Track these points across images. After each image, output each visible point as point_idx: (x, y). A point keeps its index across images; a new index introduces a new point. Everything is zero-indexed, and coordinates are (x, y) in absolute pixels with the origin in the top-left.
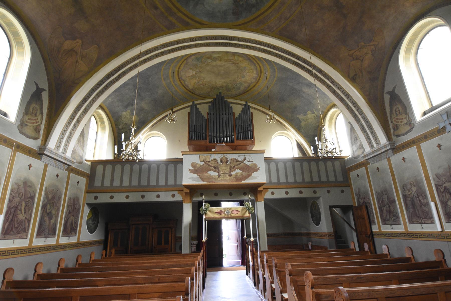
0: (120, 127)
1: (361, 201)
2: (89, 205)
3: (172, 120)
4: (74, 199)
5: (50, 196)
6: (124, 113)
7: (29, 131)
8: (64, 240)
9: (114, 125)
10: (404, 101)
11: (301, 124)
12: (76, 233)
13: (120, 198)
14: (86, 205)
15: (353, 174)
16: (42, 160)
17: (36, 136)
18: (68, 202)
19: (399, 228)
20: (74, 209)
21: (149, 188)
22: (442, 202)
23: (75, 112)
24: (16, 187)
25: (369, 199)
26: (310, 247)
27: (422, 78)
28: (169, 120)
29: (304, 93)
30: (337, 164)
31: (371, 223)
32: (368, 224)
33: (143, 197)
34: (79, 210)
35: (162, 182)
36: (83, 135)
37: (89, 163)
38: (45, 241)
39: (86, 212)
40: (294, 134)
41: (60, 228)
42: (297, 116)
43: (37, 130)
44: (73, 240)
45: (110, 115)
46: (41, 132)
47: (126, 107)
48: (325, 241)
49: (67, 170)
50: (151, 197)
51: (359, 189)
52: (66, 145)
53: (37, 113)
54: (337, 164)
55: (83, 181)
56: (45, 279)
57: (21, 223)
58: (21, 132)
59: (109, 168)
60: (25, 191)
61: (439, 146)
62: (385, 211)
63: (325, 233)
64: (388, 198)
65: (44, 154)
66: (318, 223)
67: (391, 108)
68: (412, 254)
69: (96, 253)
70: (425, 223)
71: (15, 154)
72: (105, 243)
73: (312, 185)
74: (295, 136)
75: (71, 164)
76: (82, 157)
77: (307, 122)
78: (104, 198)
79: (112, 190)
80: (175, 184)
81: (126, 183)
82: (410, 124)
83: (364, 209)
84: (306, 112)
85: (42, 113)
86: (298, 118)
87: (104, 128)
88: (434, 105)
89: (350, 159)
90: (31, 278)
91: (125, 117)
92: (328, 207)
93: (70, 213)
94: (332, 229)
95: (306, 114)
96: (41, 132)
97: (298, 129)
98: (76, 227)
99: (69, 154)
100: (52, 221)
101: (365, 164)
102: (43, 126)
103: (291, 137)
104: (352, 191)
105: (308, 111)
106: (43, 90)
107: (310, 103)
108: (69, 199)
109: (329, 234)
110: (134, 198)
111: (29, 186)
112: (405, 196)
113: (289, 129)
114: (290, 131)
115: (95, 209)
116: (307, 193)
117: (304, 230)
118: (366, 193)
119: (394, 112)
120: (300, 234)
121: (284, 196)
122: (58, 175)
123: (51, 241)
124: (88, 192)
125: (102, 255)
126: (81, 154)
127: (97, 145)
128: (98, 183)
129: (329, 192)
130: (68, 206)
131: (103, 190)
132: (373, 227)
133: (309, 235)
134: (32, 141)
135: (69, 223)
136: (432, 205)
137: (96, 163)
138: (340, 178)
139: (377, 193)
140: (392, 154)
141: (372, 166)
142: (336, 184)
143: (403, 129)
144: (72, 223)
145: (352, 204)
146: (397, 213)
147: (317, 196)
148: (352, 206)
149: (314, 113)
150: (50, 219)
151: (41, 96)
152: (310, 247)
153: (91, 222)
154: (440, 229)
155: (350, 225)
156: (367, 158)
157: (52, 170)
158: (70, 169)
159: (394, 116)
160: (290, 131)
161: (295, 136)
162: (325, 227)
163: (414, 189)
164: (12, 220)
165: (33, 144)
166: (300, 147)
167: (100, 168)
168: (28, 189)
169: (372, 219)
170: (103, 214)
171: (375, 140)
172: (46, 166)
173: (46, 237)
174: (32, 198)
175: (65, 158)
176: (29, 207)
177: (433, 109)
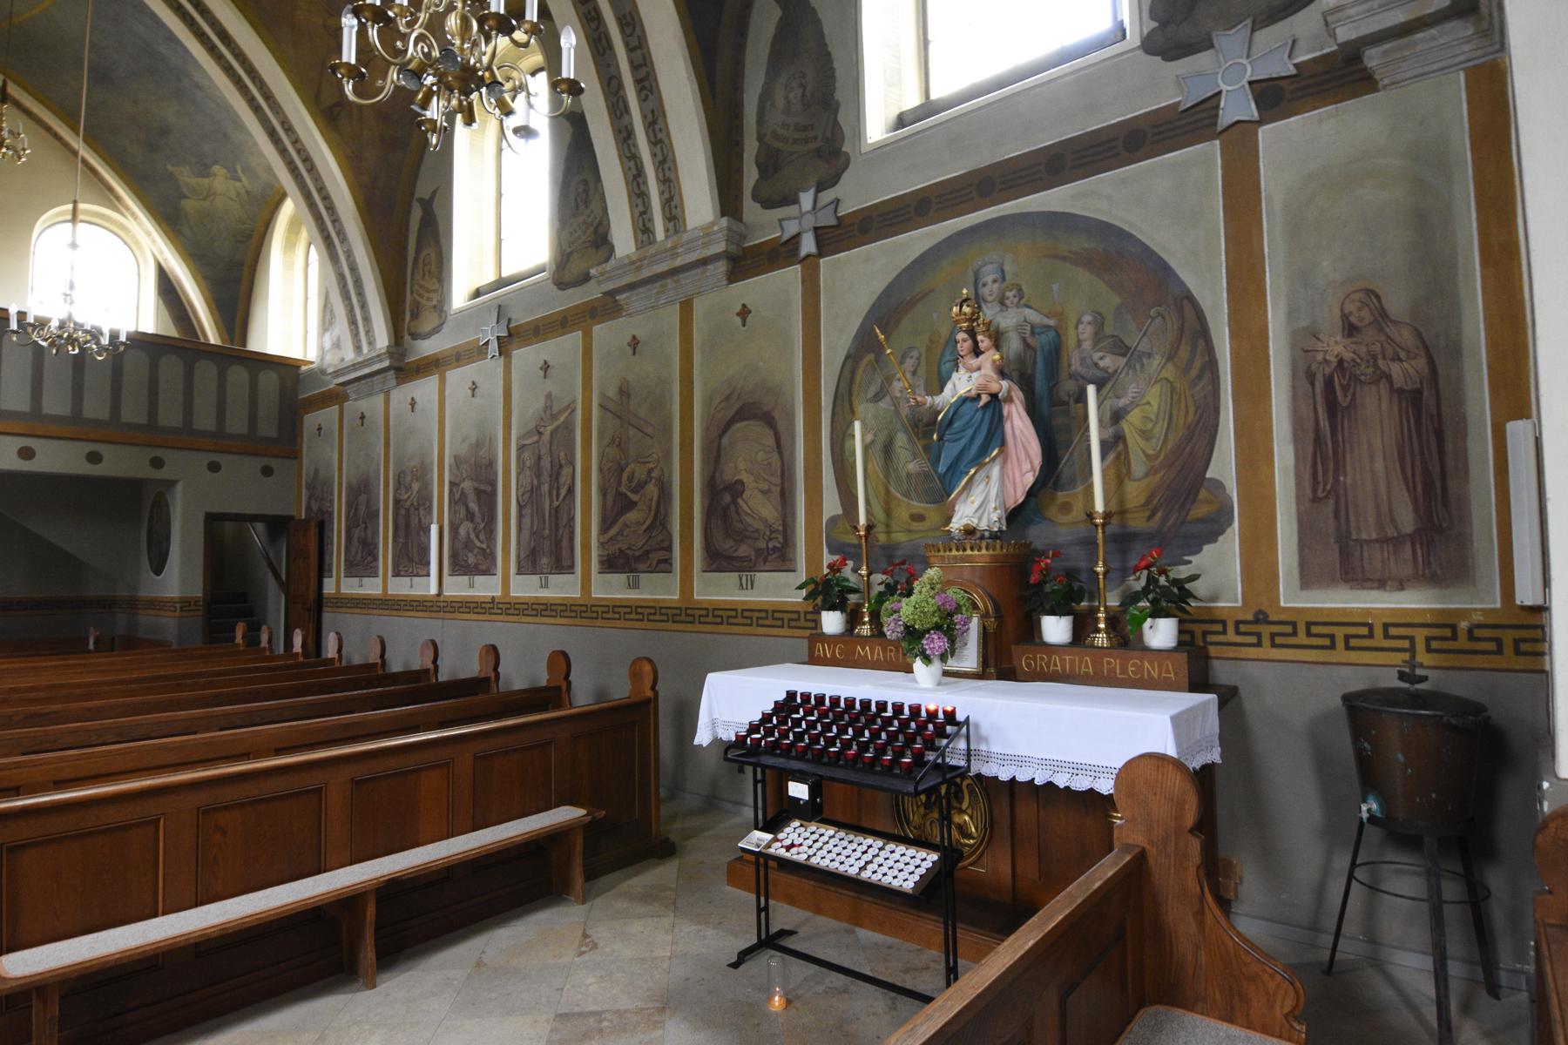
1: (315, 507)
10: (443, 240)
11: (184, 202)
15: (311, 420)
19: (429, 586)
22: (451, 523)
25: (332, 501)
26: (91, 646)
27: (499, 195)
29: (198, 86)
30: (269, 380)
31: (322, 570)
32: (313, 574)
40: (148, 234)
42: (170, 168)
48: (168, 626)
51: (316, 472)
54: (269, 380)
61: (474, 388)
62: (355, 540)
63: (172, 601)
64: (368, 506)
66: (158, 570)
67: (418, 251)
68: (382, 656)
70: (418, 575)
73: (149, 435)
74: (154, 241)
77: (207, 203)
82: (442, 311)
83: (314, 531)
84: (207, 166)
86: (171, 177)
88: (504, 275)
89: (311, 373)
92: (202, 517)
94: (201, 585)
95: (204, 170)
97: (169, 217)
101: (336, 397)
103: (137, 242)
104: (300, 474)
105: (216, 163)
107: (225, 136)
109: (186, 603)
112: (397, 502)
113: (128, 208)
114: (136, 218)
116: (119, 463)
117: (122, 592)
118: (328, 484)
119: (421, 265)
120: (109, 604)
121: (81, 467)
129: (214, 467)
132: (326, 581)
133: (133, 604)
136: (434, 529)
138: (268, 428)
139: (349, 486)
140: (394, 382)
141: (355, 406)
142: (250, 445)
143: (427, 323)
145: (293, 512)
146: (376, 546)
147: (164, 477)
148: (292, 518)
149: (239, 180)
152: (91, 646)
154: (433, 590)
155: (277, 576)
156: (341, 380)
159: (418, 276)
160: (136, 218)
161: (154, 241)
162: (179, 578)
163: (416, 486)
166: (167, 288)
169: (327, 558)
171: (367, 333)
177: (501, 283)
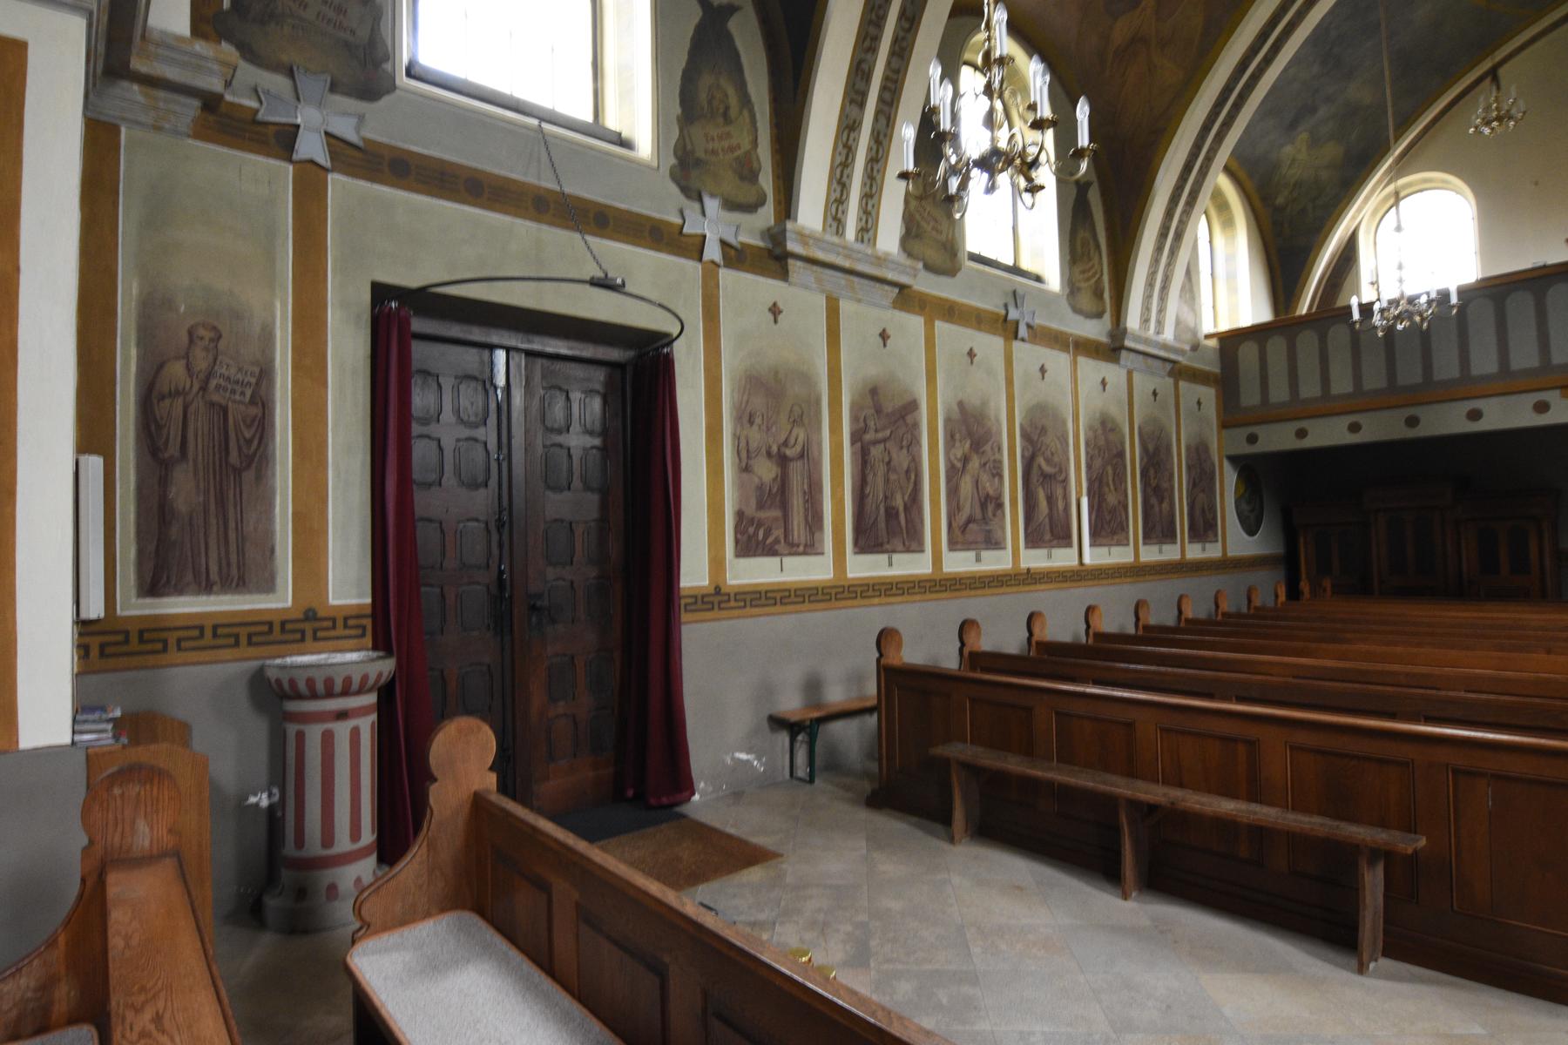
0: (1280, 200)
2: (1233, 459)
3: (1499, 119)
4: (1197, 449)
5: (1151, 447)
6: (1288, 150)
7: (1086, 301)
8: (1195, 552)
9: (1258, 203)
12: (1216, 535)
13: (1330, 433)
14: (1226, 463)
16: (1122, 362)
17: (752, 199)
18: (1188, 457)
20: (1202, 478)
21: (1432, 392)
23: (1169, 214)
24: (1091, 434)
28: (1487, 123)
33: (1412, 422)
34: (1213, 472)
35: (1485, 362)
36: (1191, 274)
37: (1213, 343)
38: (978, 559)
39: (1228, 481)
41: (1182, 523)
43: (748, 173)
44: (1213, 551)
45: (1249, 185)
46: (1107, 295)
47: (1293, 125)
49: (1171, 374)
50: (1448, 420)
52: (1161, 310)
53: (727, 108)
55: (1208, 394)
56: (1049, 657)
57: (1113, 511)
58: (1077, 310)
59: (1277, 346)
60: (1107, 440)
65: (1122, 347)
69: (1268, 589)
71: (1075, 363)
72: (1289, 563)
75: (1180, 358)
76: (1194, 332)
78: (1278, 438)
79: (1298, 411)
80: (1546, 365)
81: (1342, 384)
85: (1098, 247)
87: (1228, 223)
90: (1131, 630)
91: (1294, 160)
93: (1194, 485)
96: (1107, 295)
98: (1215, 518)
99: (1168, 335)
100: (1165, 505)
102: (1106, 278)
106: (731, 10)
108: (1188, 448)
110: (1379, 428)
111: (1112, 430)
115: (1252, 470)
122: (1155, 394)
123: (1063, 558)
124: (1225, 425)
125: (1277, 596)
126: (1192, 325)
127: (1219, 281)
128: (1250, 396)
130: (1189, 468)
131: (1269, 415)
134: (1094, 322)
135: (1198, 512)
137: (1232, 340)
144: (1203, 511)
150: (1161, 502)
151: (729, 38)
153: (1244, 506)
157: (1144, 384)
158: (1179, 372)
164: (1100, 506)
165: (1095, 330)
167: (1248, 352)
168: (1112, 437)
170: (1288, 488)
172: (1130, 373)
173: (1050, 545)
174: (1121, 454)
175: (1165, 347)
176: (1120, 477)
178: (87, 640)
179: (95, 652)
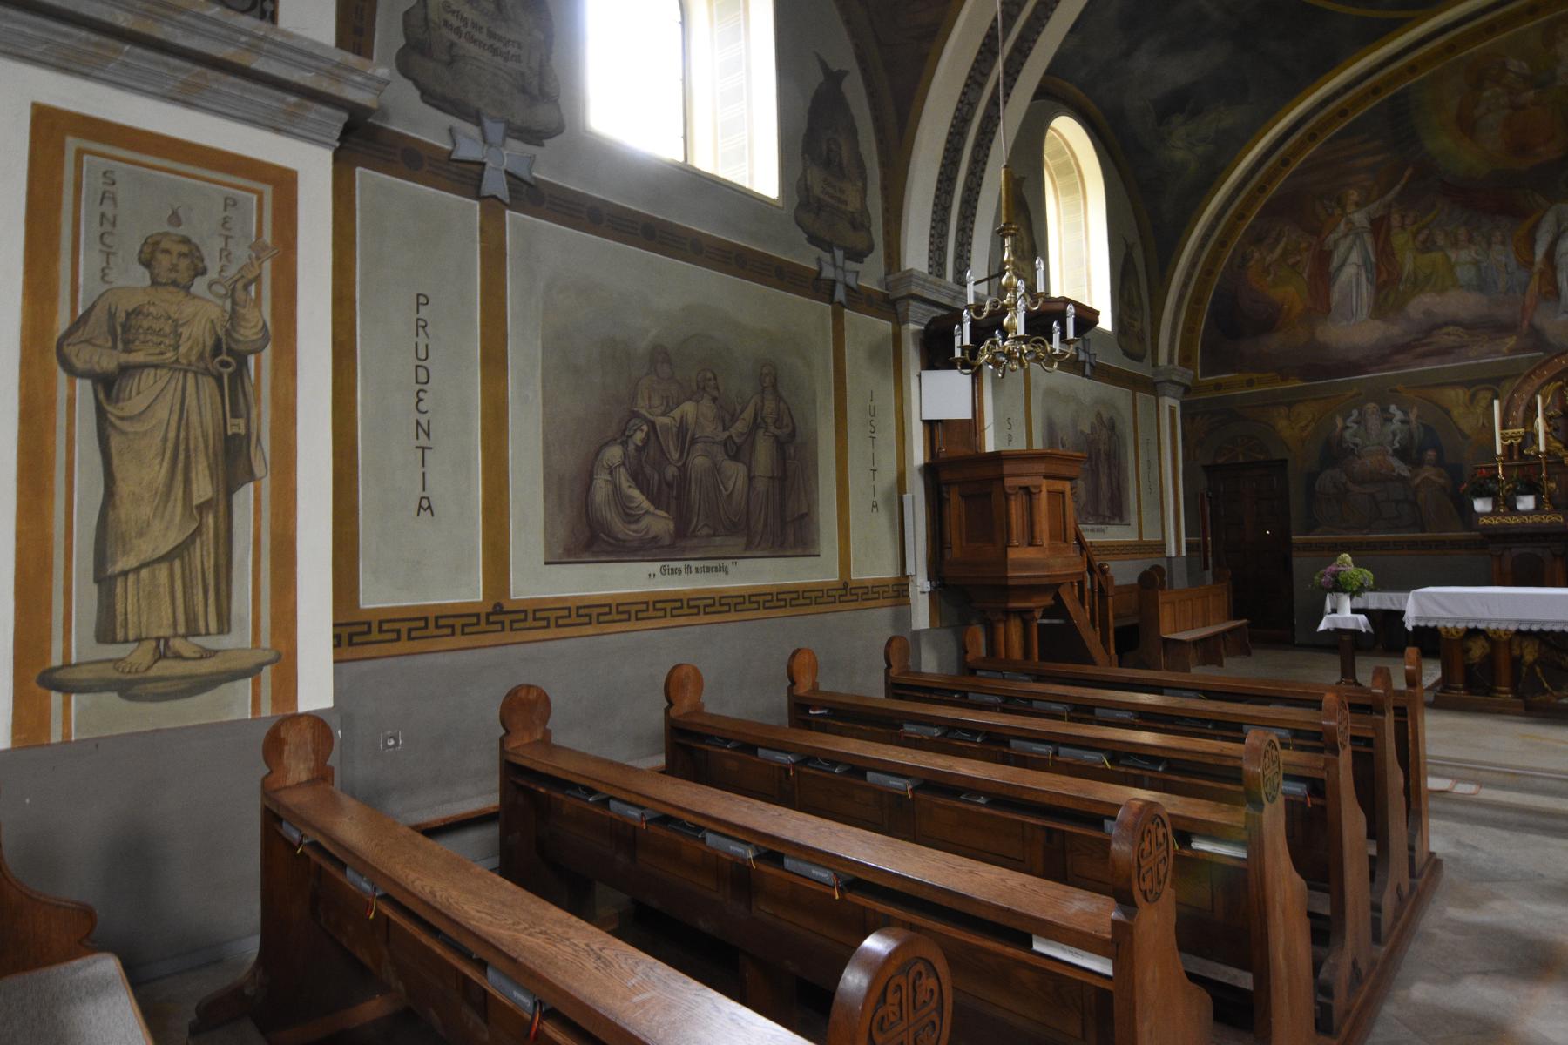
178: (339, 630)
179: (345, 640)
